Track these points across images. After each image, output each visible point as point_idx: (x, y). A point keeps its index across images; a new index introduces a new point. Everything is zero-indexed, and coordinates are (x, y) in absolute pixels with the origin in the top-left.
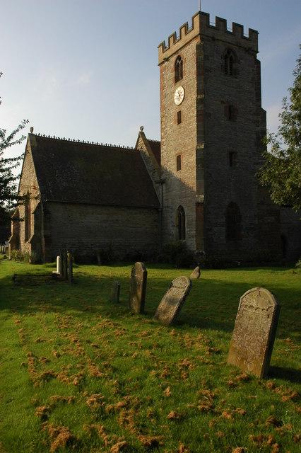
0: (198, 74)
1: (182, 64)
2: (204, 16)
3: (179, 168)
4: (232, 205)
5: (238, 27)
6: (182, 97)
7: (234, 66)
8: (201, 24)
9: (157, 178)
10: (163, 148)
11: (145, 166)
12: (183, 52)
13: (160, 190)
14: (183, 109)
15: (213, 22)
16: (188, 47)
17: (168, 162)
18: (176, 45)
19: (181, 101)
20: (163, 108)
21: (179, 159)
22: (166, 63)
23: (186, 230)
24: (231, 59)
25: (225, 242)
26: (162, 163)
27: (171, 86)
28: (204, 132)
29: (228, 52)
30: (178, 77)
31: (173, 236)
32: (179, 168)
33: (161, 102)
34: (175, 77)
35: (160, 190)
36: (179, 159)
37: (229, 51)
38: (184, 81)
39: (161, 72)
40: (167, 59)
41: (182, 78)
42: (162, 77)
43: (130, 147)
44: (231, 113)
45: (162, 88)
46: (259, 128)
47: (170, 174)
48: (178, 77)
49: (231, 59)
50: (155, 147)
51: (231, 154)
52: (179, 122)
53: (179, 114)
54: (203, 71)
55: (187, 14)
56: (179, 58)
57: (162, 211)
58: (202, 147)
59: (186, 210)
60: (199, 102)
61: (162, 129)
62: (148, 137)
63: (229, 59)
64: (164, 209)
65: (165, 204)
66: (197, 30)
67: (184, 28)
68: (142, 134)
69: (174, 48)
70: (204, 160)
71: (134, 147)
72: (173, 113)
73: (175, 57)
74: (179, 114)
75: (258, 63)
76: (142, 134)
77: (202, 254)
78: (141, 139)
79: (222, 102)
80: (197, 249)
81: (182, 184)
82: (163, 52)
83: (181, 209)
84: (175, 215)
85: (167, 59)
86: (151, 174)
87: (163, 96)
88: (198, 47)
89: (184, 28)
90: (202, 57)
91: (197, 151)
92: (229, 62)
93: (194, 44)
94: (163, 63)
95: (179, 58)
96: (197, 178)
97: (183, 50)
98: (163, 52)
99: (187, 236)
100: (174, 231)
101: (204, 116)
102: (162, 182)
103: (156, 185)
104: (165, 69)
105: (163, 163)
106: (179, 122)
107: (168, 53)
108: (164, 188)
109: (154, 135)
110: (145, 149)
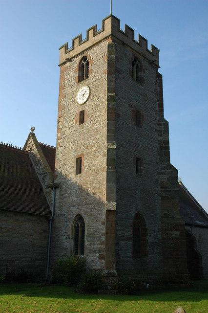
0: (109, 73)
1: (88, 64)
2: (116, 21)
3: (79, 170)
4: (138, 216)
5: (143, 40)
6: (87, 96)
7: (139, 74)
8: (113, 27)
9: (48, 181)
10: (59, 156)
11: (34, 169)
12: (90, 54)
13: (53, 195)
14: (88, 109)
15: (123, 28)
16: (96, 48)
17: (65, 165)
18: (82, 46)
19: (85, 100)
20: (61, 108)
21: (79, 162)
22: (68, 64)
23: (86, 243)
24: (137, 67)
25: (131, 259)
26: (57, 166)
27: (73, 86)
28: (114, 132)
29: (135, 60)
30: (83, 73)
31: (66, 249)
32: (79, 170)
33: (60, 102)
34: (79, 77)
35: (52, 197)
36: (79, 162)
37: (136, 59)
38: (91, 78)
39: (62, 72)
40: (69, 60)
41: (88, 77)
42: (62, 77)
43: (18, 147)
44: (138, 118)
45: (62, 87)
46: (162, 138)
47: (65, 178)
48: (83, 73)
49: (137, 67)
50: (49, 153)
51: (138, 160)
52: (82, 121)
53: (82, 114)
54: (114, 70)
55: (98, 16)
56: (84, 59)
57: (53, 220)
58: (114, 146)
59: (86, 220)
60: (110, 99)
61: (58, 129)
62: (41, 140)
63: (135, 67)
64: (56, 218)
65: (58, 211)
66: (108, 30)
67: (92, 30)
68: (32, 135)
69: (79, 49)
70: (114, 161)
71: (22, 148)
72: (74, 112)
73: (80, 57)
74: (82, 114)
75: (160, 77)
76: (32, 135)
77: (113, 275)
78: (31, 140)
79: (130, 106)
80: (107, 268)
81: (81, 191)
82: (66, 53)
83: (80, 218)
84: (71, 225)
85: (69, 60)
86: (40, 178)
87: (62, 96)
88: (109, 46)
89: (92, 30)
90: (113, 56)
91: (108, 150)
92: (135, 69)
93: (105, 45)
94: (65, 63)
95: (84, 59)
96: (108, 181)
97: (90, 52)
98: (66, 53)
99: (86, 251)
100: (67, 243)
101: (113, 115)
102: (56, 187)
103: (46, 190)
104: (66, 69)
105: (58, 166)
106: (82, 121)
107: (71, 54)
108: (58, 193)
109: (48, 138)
110: (35, 150)
